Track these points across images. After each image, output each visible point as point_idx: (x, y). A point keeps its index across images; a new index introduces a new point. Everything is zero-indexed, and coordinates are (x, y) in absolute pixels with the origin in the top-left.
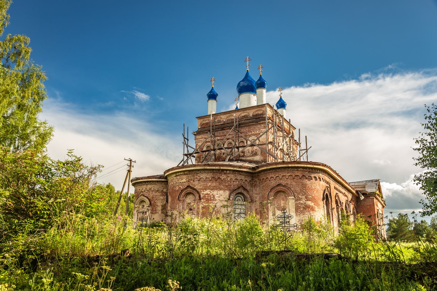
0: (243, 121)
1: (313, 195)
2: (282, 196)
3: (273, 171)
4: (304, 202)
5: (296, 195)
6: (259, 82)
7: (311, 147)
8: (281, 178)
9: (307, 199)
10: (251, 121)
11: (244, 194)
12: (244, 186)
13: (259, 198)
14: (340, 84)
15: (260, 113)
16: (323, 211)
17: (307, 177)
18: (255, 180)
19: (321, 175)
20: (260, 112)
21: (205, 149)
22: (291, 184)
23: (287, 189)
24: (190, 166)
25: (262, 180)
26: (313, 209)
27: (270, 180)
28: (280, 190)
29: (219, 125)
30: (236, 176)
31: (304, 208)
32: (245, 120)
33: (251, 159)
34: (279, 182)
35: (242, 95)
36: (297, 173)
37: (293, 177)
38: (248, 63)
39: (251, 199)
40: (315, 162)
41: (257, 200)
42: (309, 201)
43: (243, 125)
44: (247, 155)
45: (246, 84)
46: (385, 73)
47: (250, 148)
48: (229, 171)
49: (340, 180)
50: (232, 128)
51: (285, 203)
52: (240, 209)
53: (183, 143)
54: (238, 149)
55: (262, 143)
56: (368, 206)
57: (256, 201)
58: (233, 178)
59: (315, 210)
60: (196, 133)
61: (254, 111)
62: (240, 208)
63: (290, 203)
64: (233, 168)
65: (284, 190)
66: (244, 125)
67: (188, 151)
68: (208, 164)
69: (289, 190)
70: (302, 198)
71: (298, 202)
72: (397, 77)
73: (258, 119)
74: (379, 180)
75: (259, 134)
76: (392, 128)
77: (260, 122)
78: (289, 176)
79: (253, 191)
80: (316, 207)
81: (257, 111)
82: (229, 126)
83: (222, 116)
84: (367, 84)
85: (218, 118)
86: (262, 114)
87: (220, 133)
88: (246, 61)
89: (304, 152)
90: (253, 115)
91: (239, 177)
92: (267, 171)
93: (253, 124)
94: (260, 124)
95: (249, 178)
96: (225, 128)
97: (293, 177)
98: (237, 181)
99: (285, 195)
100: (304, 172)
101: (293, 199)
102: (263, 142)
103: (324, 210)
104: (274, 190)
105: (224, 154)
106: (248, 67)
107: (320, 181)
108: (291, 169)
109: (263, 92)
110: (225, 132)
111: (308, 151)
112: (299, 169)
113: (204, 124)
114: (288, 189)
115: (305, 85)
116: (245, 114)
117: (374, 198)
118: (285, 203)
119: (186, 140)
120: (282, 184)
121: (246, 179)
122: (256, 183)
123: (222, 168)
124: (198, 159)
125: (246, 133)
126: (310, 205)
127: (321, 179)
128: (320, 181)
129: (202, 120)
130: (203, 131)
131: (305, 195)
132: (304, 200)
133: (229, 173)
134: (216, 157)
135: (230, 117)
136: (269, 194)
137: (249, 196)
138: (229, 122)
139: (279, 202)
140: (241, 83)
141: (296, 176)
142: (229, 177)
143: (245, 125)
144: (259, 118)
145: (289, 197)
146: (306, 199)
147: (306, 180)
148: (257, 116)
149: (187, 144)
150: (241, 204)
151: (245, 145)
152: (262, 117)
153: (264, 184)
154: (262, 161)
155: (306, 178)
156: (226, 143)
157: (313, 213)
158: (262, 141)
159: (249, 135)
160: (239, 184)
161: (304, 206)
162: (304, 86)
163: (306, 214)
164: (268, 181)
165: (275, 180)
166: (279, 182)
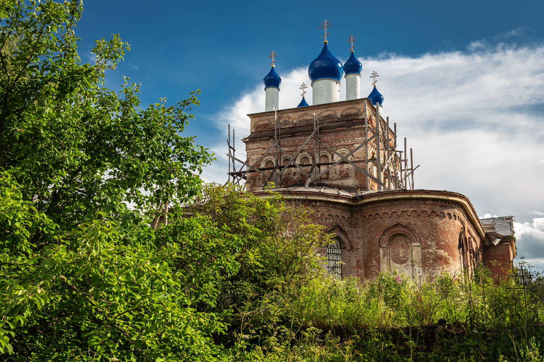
0: (325, 124)
1: (447, 241)
2: (401, 241)
3: (388, 204)
4: (434, 251)
5: (423, 240)
6: (351, 63)
7: (419, 166)
8: (399, 214)
9: (439, 247)
10: (338, 124)
11: (340, 238)
12: (340, 225)
13: (362, 243)
14: (436, 57)
15: (353, 112)
16: (460, 264)
17: (438, 214)
18: (356, 216)
19: (456, 210)
20: (353, 111)
21: (263, 166)
22: (415, 224)
23: (409, 232)
24: (259, 194)
25: (367, 217)
26: (447, 262)
27: (382, 218)
28: (398, 232)
29: (286, 128)
30: (329, 210)
31: (434, 260)
32: (329, 122)
33: (340, 184)
34: (396, 221)
35: (318, 82)
36: (423, 208)
37: (418, 213)
38: (326, 30)
39: (350, 245)
40: (450, 192)
41: (359, 247)
42: (441, 249)
43: (326, 131)
44: (333, 177)
45: (324, 65)
46: (506, 43)
47: (338, 167)
48: (320, 203)
49: (474, 218)
50: (311, 134)
51: (406, 252)
52: (335, 260)
53: (227, 155)
54: (319, 168)
55: (357, 159)
56: (500, 256)
57: (357, 249)
58: (325, 214)
59: (449, 263)
60: (248, 140)
61: (344, 108)
62: (334, 259)
63: (414, 253)
64: (326, 197)
65: (405, 233)
66: (328, 130)
67: (234, 169)
68: (289, 191)
69: (412, 233)
70: (431, 246)
71: (426, 251)
72: (523, 51)
73: (351, 123)
74: (512, 217)
75: (353, 145)
76: (512, 131)
77: (355, 127)
78: (413, 211)
79: (352, 234)
80: (451, 258)
81: (347, 109)
82: (303, 130)
83: (291, 115)
84: (478, 59)
85: (285, 117)
86: (357, 115)
87: (288, 142)
88: (323, 27)
89: (410, 171)
90: (342, 116)
91: (334, 212)
92: (377, 203)
93: (343, 130)
94: (353, 130)
95: (347, 213)
96: (297, 134)
97: (418, 213)
98: (331, 218)
99: (406, 240)
100: (434, 206)
101: (419, 246)
102: (358, 158)
103: (461, 262)
104: (389, 233)
105: (295, 174)
106: (326, 38)
107: (456, 219)
108: (415, 201)
109: (356, 80)
110: (297, 139)
111: (414, 172)
112: (427, 202)
113: (260, 125)
114: (411, 231)
115: (381, 55)
116: (329, 113)
117: (509, 245)
118: (406, 252)
119: (232, 151)
120: (401, 224)
121: (344, 215)
122: (358, 221)
123: (309, 198)
124: (252, 181)
125: (332, 143)
126: (443, 255)
127: (457, 216)
128: (456, 219)
129: (257, 119)
130: (259, 136)
131: (436, 241)
132: (434, 249)
133: (320, 206)
134: (282, 179)
135: (304, 117)
136: (380, 239)
137: (348, 241)
138: (302, 124)
139: (396, 251)
140: (316, 62)
141: (422, 211)
142: (319, 211)
143: (330, 130)
144: (352, 120)
145: (413, 244)
146: (437, 246)
147: (437, 219)
148: (348, 117)
149: (233, 156)
150: (336, 252)
151: (330, 162)
152: (356, 119)
153: (372, 223)
154: (357, 186)
155: (437, 215)
156: (298, 157)
157: (446, 267)
158: (357, 156)
159: (336, 146)
160: (333, 222)
161: (434, 257)
162: (379, 58)
163: (437, 268)
164: (379, 219)
165: (390, 217)
166: (396, 221)
